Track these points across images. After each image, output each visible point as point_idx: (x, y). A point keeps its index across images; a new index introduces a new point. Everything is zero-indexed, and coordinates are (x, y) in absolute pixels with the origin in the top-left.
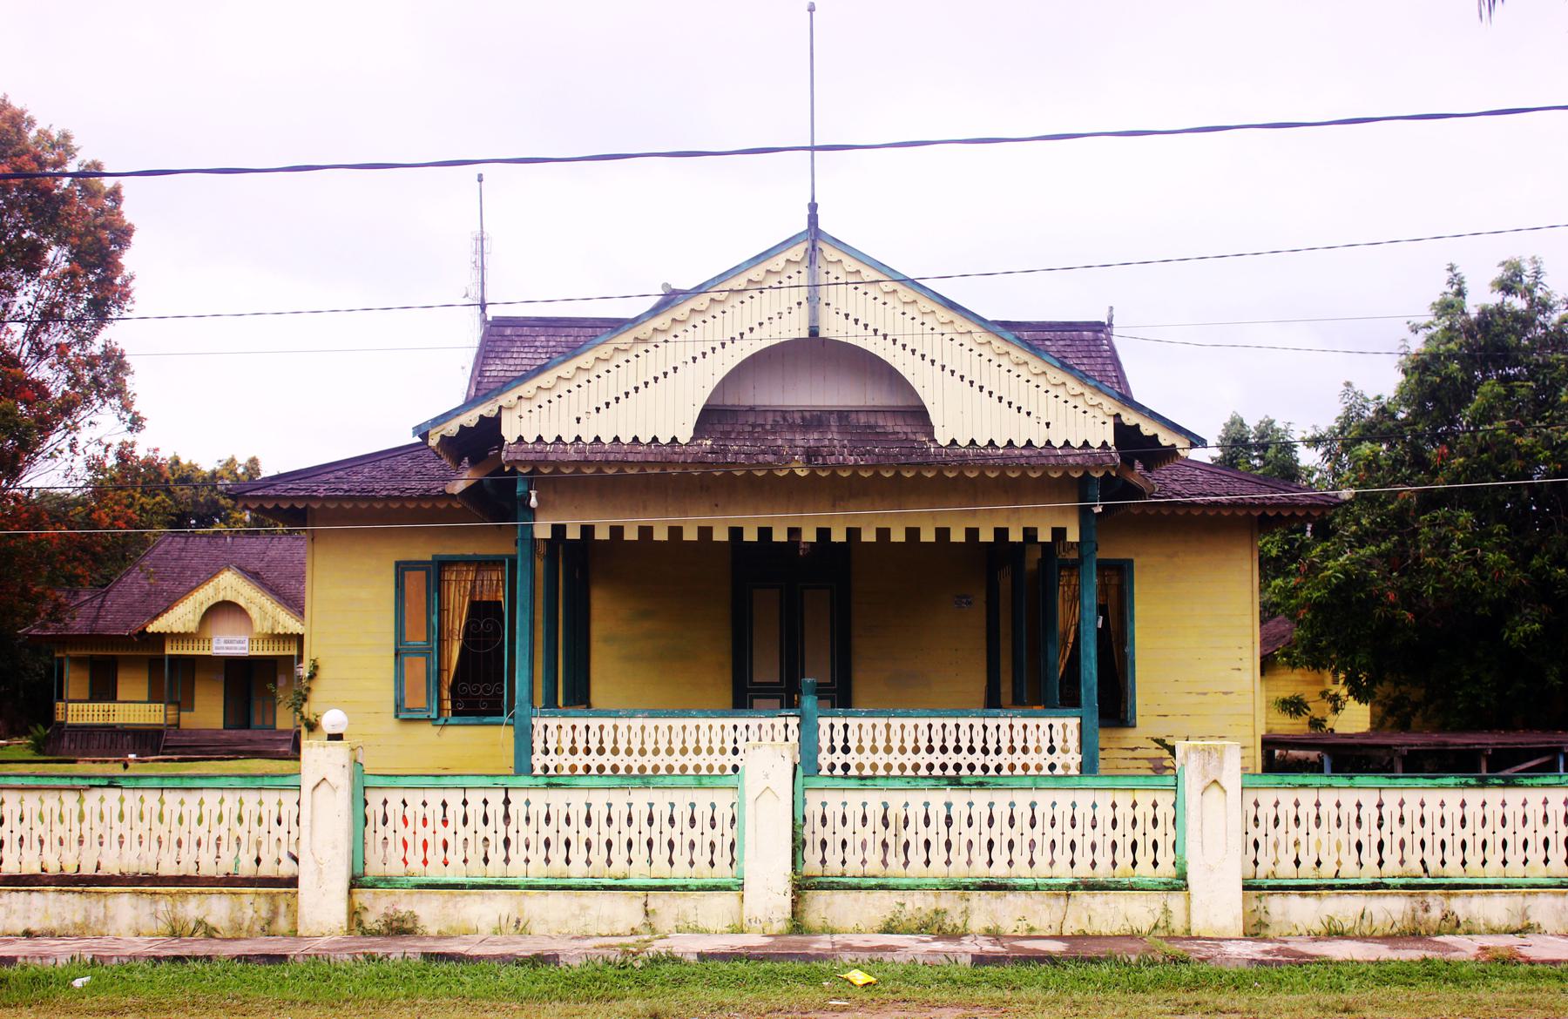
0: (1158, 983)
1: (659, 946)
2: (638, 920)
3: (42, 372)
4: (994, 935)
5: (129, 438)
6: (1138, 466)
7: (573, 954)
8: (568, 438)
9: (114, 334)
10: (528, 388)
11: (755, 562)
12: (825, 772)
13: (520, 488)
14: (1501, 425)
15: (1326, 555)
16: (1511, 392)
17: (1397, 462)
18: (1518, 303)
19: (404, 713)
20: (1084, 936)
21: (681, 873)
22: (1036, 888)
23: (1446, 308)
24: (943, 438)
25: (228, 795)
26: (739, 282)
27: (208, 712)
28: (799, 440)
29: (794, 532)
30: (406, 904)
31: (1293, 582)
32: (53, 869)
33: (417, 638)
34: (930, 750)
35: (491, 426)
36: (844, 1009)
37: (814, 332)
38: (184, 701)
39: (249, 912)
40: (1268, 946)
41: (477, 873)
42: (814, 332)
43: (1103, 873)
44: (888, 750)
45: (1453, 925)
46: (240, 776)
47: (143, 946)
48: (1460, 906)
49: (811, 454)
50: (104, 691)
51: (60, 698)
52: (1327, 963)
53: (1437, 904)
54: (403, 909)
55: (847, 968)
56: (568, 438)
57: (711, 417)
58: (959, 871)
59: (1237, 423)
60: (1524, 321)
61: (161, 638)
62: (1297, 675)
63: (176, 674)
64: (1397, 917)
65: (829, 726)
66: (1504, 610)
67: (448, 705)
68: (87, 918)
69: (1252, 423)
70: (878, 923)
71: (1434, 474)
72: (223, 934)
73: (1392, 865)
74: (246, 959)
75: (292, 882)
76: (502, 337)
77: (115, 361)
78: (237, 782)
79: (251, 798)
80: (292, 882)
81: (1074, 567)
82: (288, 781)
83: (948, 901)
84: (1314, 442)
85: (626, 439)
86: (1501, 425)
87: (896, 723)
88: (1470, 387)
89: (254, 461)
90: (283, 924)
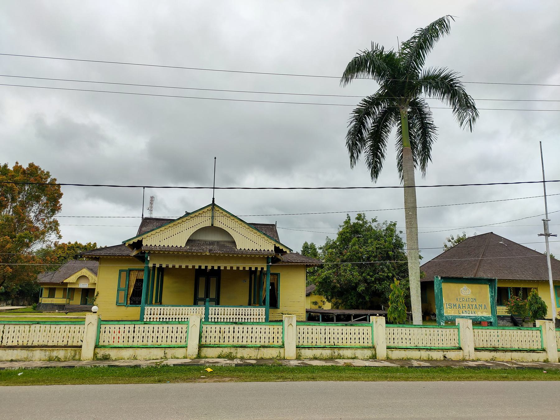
0: (275, 371)
1: (165, 363)
2: (163, 355)
3: (37, 225)
4: (242, 358)
5: (58, 240)
6: (280, 255)
7: (144, 364)
8: (157, 245)
9: (57, 217)
10: (149, 234)
11: (200, 273)
12: (210, 320)
13: (146, 255)
14: (357, 247)
15: (322, 272)
16: (359, 240)
17: (337, 253)
18: (361, 222)
19: (118, 304)
20: (262, 359)
21: (174, 344)
22: (252, 347)
23: (347, 222)
24: (238, 248)
25: (67, 326)
26: (197, 214)
27: (77, 300)
28: (208, 247)
29: (206, 267)
30: (107, 352)
31: (315, 277)
32: (21, 344)
33: (123, 286)
34: (233, 315)
35: (140, 242)
36: (204, 378)
37: (212, 225)
38: (71, 298)
39: (69, 354)
40: (300, 362)
41: (126, 344)
42: (212, 225)
43: (267, 344)
44: (224, 314)
45: (340, 357)
46: (23, 347)
47: (39, 364)
48: (342, 352)
49: (210, 251)
50: (51, 295)
51: (41, 297)
52: (311, 366)
53: (337, 352)
54: (107, 353)
55: (207, 367)
56: (157, 245)
57: (189, 242)
58: (236, 343)
59: (306, 243)
60: (362, 226)
61: (67, 284)
62: (317, 296)
63: (70, 292)
64: (328, 354)
65: (212, 309)
66: (357, 285)
67: (129, 302)
68: (28, 356)
69: (309, 243)
70: (217, 356)
71: (344, 256)
72: (63, 360)
73: (327, 343)
74: (64, 367)
75: (81, 347)
76: (146, 222)
77: (56, 223)
78: (70, 323)
79: (73, 327)
80: (81, 347)
81: (266, 274)
82: (83, 323)
83: (233, 350)
84: (321, 248)
85: (170, 246)
86: (357, 247)
87: (226, 308)
88: (351, 238)
89: (95, 243)
90: (77, 357)
